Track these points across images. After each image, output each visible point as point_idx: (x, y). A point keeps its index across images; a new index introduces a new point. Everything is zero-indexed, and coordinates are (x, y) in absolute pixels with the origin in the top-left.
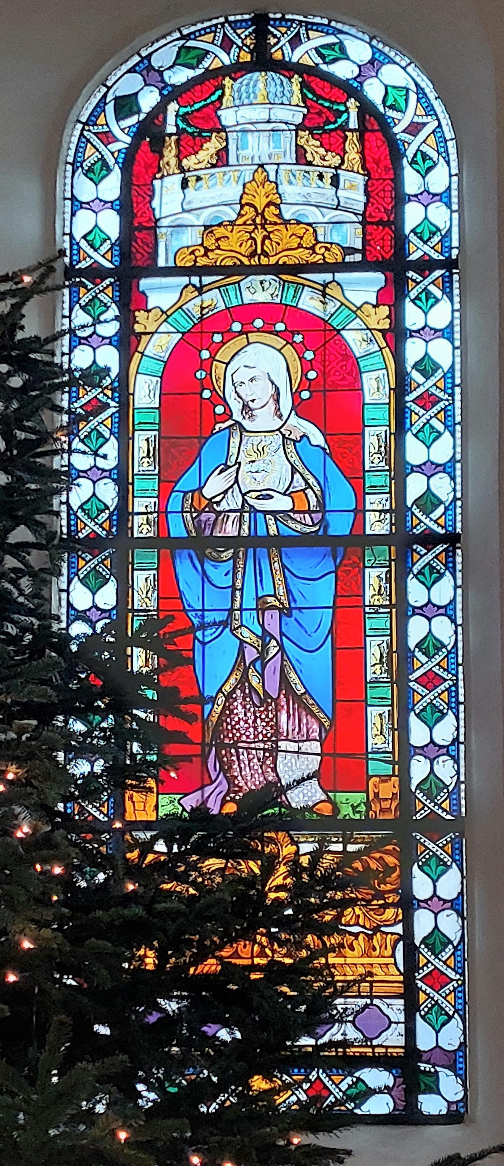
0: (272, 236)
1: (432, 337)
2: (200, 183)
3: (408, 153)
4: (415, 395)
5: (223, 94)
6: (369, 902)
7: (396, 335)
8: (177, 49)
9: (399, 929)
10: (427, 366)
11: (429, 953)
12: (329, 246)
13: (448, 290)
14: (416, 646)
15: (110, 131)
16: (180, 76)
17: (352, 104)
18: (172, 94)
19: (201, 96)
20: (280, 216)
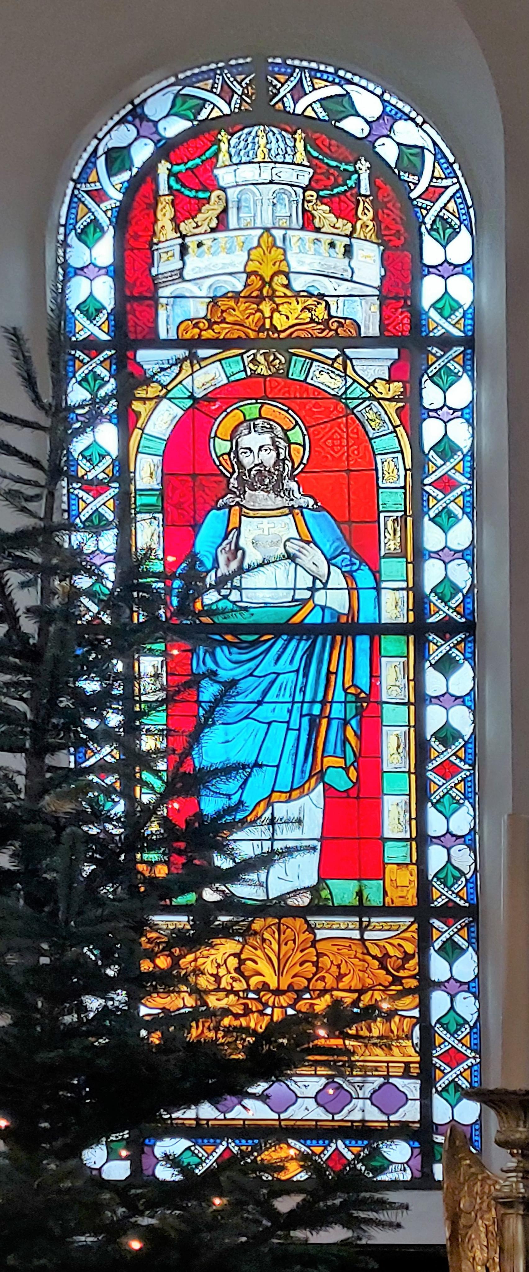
0: (281, 308)
1: (452, 417)
2: (201, 249)
3: (426, 220)
4: (433, 477)
5: (219, 150)
6: (386, 988)
7: (412, 414)
8: (172, 97)
9: (416, 1013)
10: (445, 447)
11: (442, 886)
12: (343, 321)
13: (469, 368)
14: (432, 591)
15: (102, 189)
16: (174, 127)
17: (363, 166)
18: (166, 149)
19: (195, 152)
20: (288, 286)
